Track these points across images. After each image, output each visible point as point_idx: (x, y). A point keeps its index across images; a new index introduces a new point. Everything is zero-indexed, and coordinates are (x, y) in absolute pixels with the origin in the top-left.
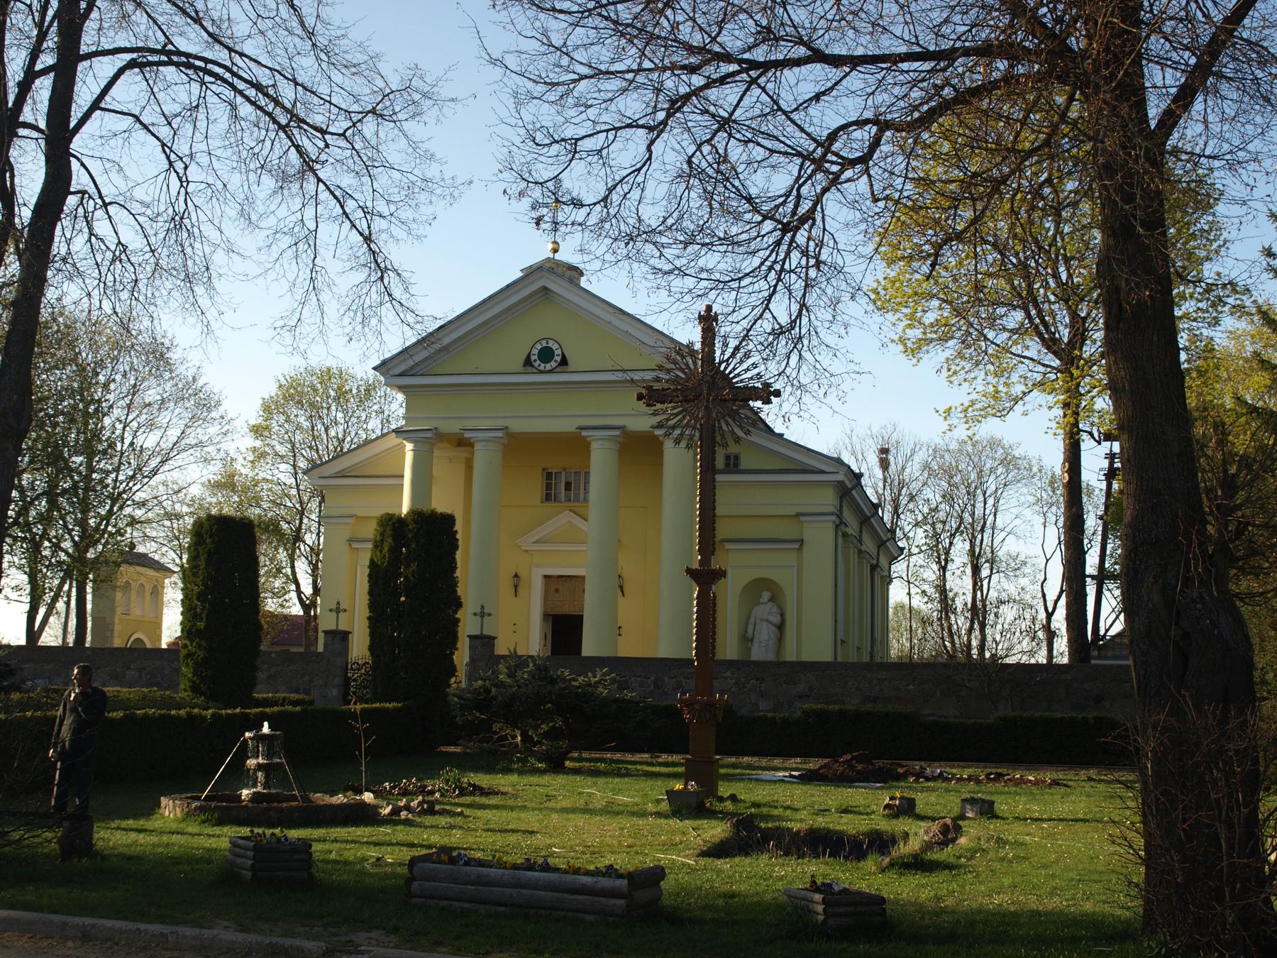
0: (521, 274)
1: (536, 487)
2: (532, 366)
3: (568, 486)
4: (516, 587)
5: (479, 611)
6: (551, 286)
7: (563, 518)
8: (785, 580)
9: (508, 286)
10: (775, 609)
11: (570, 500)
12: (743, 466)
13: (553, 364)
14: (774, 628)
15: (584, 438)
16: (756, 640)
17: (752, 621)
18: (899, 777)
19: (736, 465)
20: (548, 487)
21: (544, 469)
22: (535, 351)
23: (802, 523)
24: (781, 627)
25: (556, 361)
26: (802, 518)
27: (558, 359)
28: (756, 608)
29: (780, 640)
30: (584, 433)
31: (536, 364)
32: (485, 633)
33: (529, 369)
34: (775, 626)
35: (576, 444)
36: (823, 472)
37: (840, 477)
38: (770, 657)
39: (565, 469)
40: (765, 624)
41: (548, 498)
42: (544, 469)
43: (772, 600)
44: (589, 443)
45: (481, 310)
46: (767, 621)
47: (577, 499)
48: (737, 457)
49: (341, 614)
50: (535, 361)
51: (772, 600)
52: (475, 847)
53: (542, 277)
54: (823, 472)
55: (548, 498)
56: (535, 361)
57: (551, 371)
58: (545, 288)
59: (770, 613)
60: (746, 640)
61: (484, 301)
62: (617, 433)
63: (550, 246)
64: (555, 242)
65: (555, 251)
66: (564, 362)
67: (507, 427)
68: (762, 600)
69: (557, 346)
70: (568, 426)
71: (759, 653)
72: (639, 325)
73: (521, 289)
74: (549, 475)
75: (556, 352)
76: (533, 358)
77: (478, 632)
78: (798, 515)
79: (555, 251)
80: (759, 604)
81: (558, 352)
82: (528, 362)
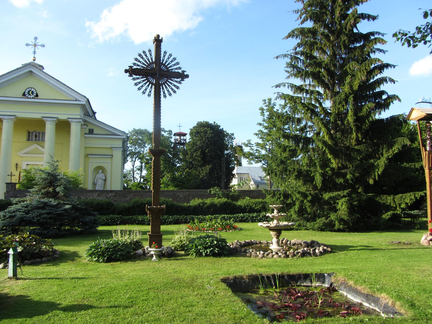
0: (21, 66)
1: (25, 137)
2: (25, 96)
3: (36, 136)
4: (17, 168)
5: (10, 174)
6: (33, 70)
7: (34, 146)
8: (107, 167)
9: (17, 69)
10: (103, 175)
11: (33, 141)
12: (94, 133)
13: (33, 96)
14: (103, 181)
15: (43, 120)
16: (97, 185)
17: (96, 178)
18: (56, 214)
19: (92, 132)
20: (29, 136)
21: (27, 131)
22: (27, 91)
23: (112, 150)
24: (105, 180)
25: (34, 95)
26: (113, 149)
27: (35, 94)
28: (98, 175)
29: (105, 184)
30: (44, 119)
31: (27, 95)
32: (12, 182)
33: (24, 97)
34: (103, 180)
35: (41, 123)
36: (119, 135)
37: (124, 137)
38: (102, 189)
39: (35, 131)
40: (100, 179)
41: (29, 140)
42: (27, 131)
43: (102, 172)
44: (45, 123)
45: (22, 69)
46: (101, 178)
47: (39, 140)
48: (93, 130)
49: (13, 177)
50: (27, 94)
51: (102, 172)
52: (87, 277)
53: (30, 67)
54: (119, 135)
55: (29, 140)
56: (27, 94)
57: (33, 98)
58: (31, 72)
59: (102, 176)
60: (94, 184)
61: (8, 73)
62: (55, 119)
63: (33, 58)
64: (34, 57)
65: (34, 60)
66: (37, 95)
67: (15, 115)
68: (99, 172)
69: (35, 90)
70: (39, 116)
71: (99, 187)
72: (64, 86)
73: (22, 71)
74: (29, 133)
75: (34, 92)
76: (26, 93)
77: (9, 182)
78: (111, 148)
79: (34, 60)
80: (98, 173)
81: (35, 92)
82: (24, 94)
